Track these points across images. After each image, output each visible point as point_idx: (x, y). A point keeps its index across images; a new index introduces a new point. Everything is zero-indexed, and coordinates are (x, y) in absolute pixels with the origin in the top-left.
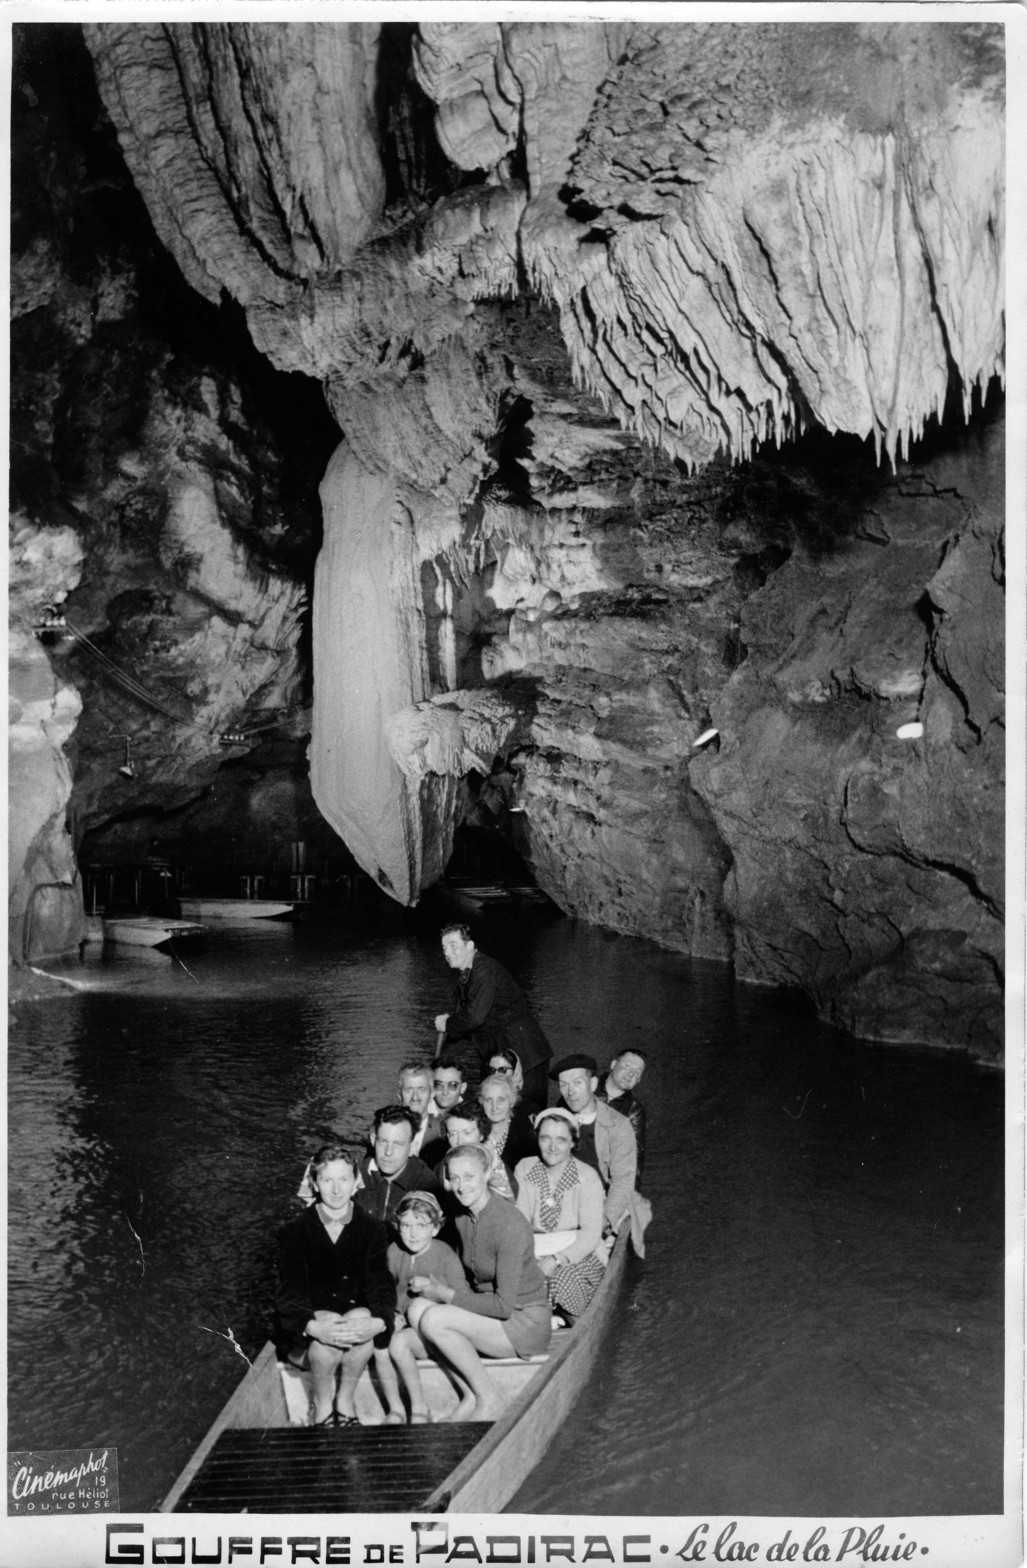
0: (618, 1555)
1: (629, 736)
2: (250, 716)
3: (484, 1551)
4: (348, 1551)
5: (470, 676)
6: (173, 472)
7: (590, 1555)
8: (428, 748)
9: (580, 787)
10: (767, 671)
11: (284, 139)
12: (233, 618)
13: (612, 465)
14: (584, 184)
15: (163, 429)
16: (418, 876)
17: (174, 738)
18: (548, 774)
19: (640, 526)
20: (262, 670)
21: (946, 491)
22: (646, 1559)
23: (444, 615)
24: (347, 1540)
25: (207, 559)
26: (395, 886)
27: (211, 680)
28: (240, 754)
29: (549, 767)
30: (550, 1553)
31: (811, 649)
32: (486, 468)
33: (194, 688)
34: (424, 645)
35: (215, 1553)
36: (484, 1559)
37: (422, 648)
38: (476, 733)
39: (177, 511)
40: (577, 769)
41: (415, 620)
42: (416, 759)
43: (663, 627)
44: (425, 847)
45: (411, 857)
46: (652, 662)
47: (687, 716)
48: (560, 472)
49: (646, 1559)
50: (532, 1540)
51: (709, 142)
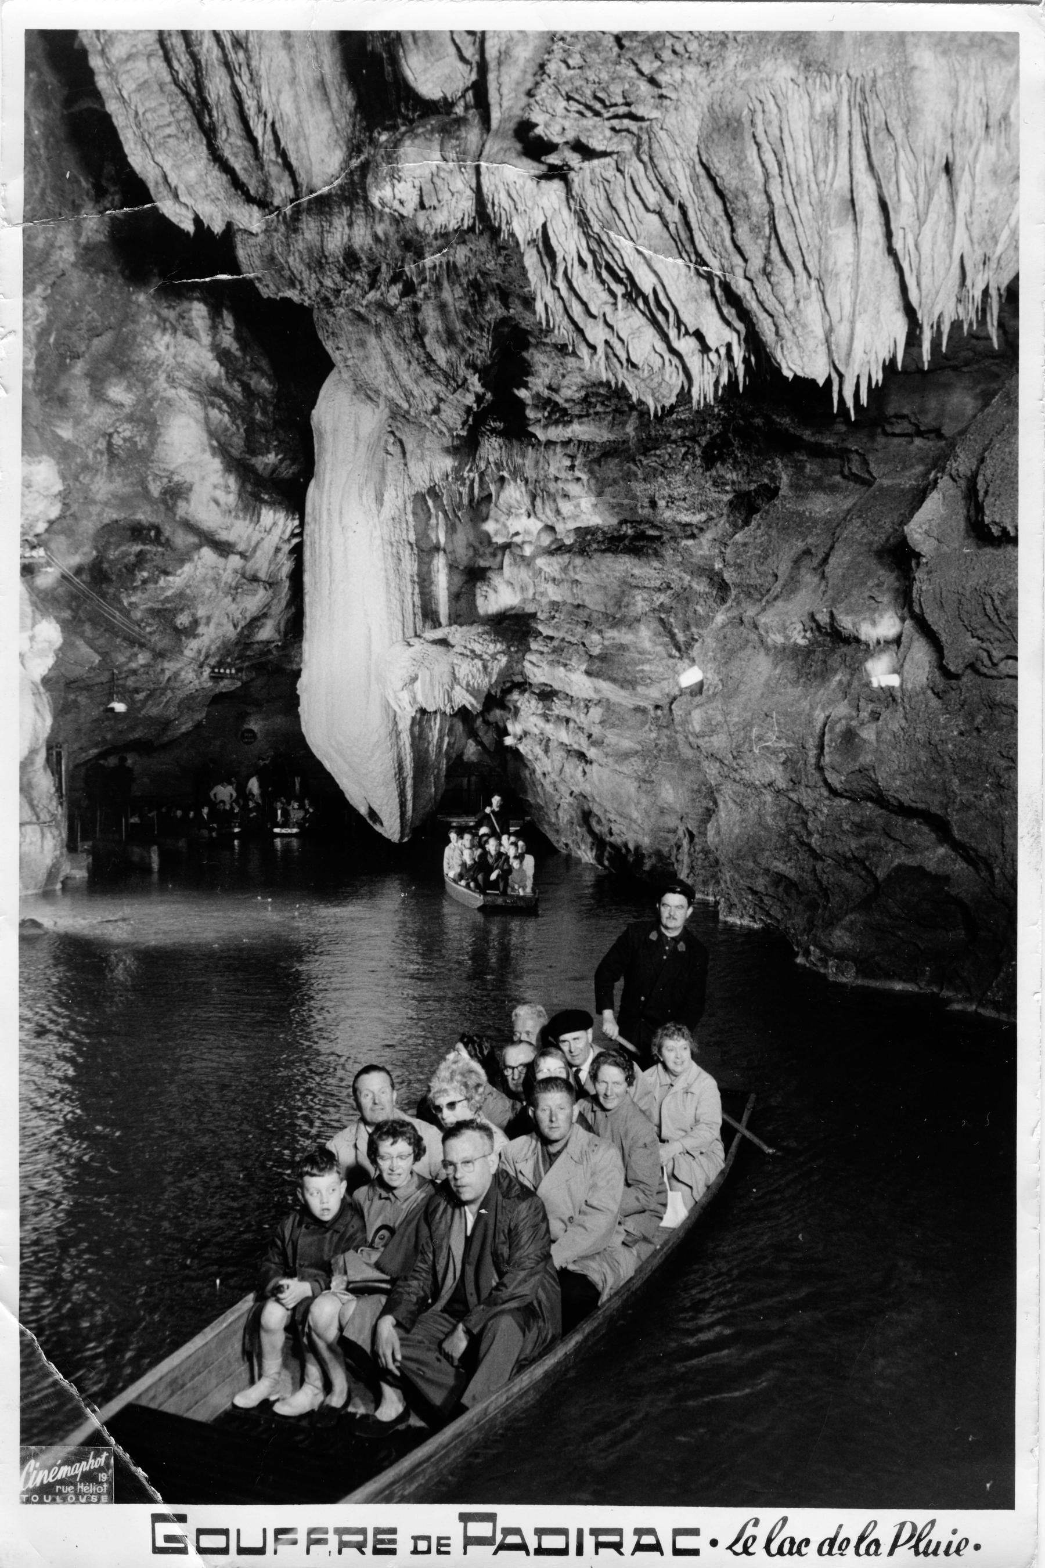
0: (667, 1547)
1: (620, 675)
2: (241, 649)
3: (532, 1543)
4: (394, 1541)
5: (464, 612)
6: (162, 399)
7: (639, 1547)
8: (418, 684)
9: (571, 725)
10: (750, 611)
11: (254, 63)
12: (223, 548)
13: (609, 398)
14: (537, 117)
15: (151, 354)
16: (409, 813)
17: (163, 670)
18: (540, 712)
19: (634, 461)
20: (253, 602)
21: (929, 431)
22: (695, 1552)
23: (437, 548)
24: (393, 1531)
25: (196, 488)
26: (385, 824)
27: (201, 612)
28: (233, 688)
29: (541, 705)
30: (599, 1545)
31: (794, 591)
32: (479, 399)
33: (183, 620)
34: (416, 579)
35: (260, 1545)
36: (532, 1551)
37: (414, 582)
38: (467, 669)
39: (167, 439)
40: (569, 707)
41: (406, 553)
42: (405, 696)
43: (656, 564)
44: (415, 786)
45: (402, 794)
46: (644, 600)
47: (677, 654)
48: (556, 404)
49: (695, 1552)
50: (580, 1532)
51: (662, 78)
